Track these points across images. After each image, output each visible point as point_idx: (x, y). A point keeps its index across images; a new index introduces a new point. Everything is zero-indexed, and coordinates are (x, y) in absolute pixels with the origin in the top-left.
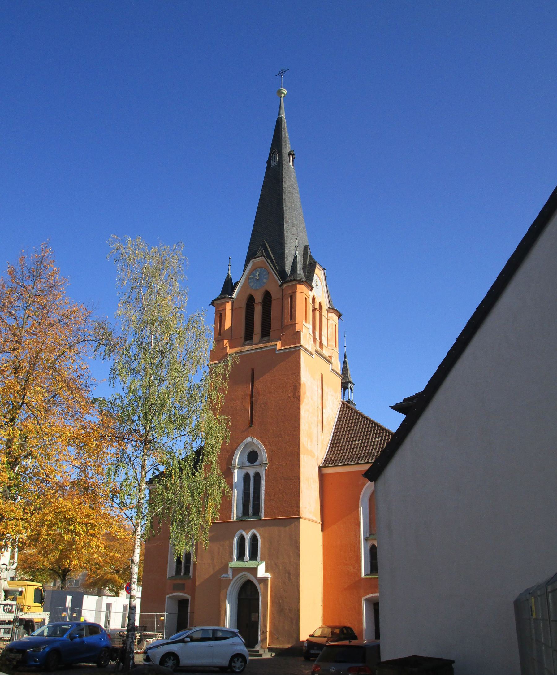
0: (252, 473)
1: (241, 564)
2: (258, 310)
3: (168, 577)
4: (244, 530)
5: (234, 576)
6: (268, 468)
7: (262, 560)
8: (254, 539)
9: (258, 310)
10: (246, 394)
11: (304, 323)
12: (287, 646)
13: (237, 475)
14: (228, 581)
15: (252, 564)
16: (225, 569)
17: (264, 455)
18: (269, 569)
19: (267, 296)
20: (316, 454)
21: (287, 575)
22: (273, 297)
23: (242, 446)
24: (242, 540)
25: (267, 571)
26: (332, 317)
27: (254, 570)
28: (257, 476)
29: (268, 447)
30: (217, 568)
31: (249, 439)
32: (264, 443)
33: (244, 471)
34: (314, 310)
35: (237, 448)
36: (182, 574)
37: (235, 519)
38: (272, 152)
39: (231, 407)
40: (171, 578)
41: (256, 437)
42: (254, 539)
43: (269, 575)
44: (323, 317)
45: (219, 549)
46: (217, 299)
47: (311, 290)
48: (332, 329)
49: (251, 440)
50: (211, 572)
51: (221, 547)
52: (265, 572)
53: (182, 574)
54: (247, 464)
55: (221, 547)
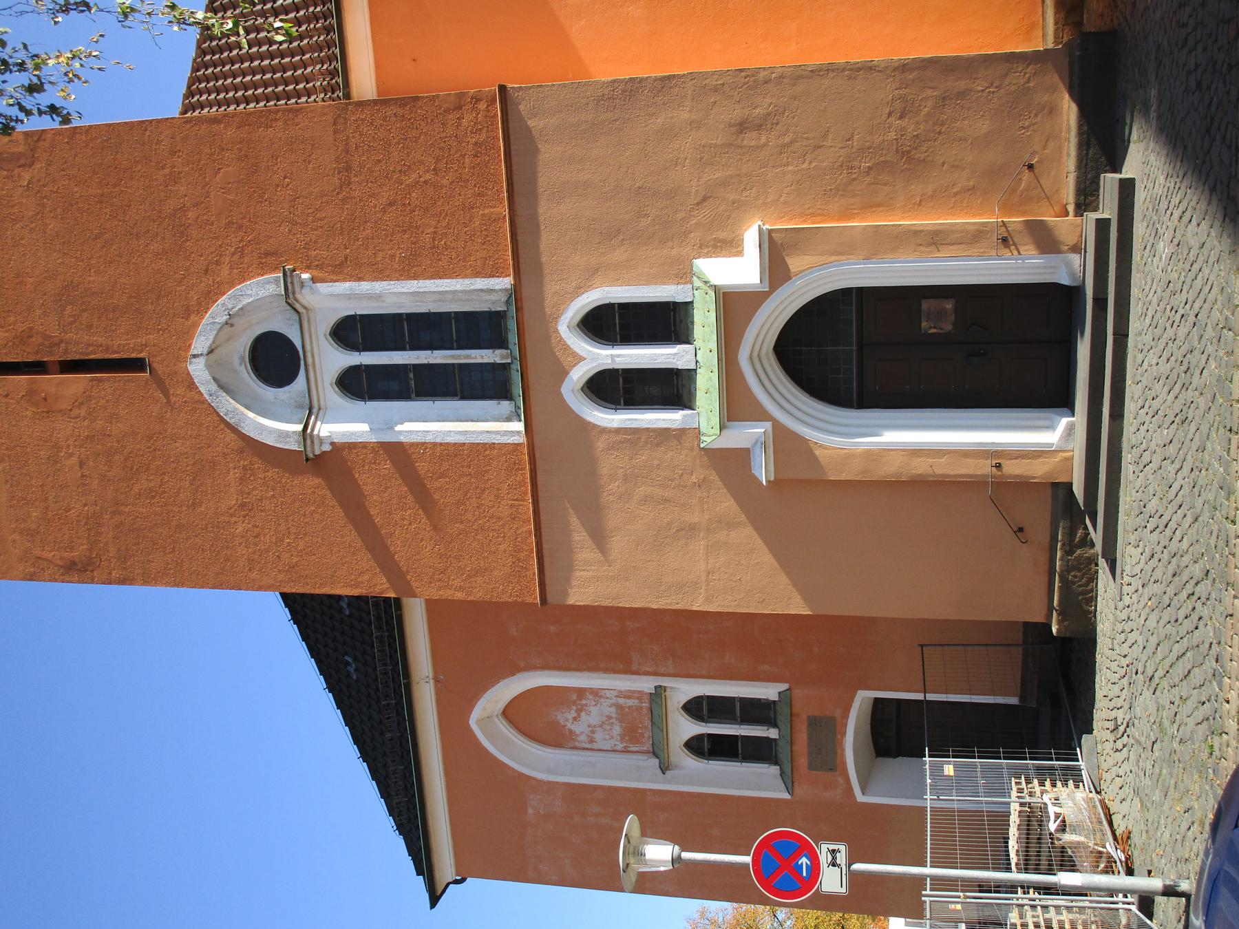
0: (341, 360)
1: (707, 386)
3: (786, 796)
4: (563, 373)
5: (760, 415)
6: (308, 268)
7: (685, 274)
8: (605, 324)
10: (31, 394)
12: (1069, 111)
13: (347, 425)
15: (704, 323)
16: (731, 464)
17: (254, 299)
18: (722, 235)
21: (750, 139)
23: (227, 405)
24: (611, 388)
25: (730, 246)
27: (734, 307)
28: (350, 332)
29: (225, 272)
30: (726, 504)
31: (198, 370)
32: (210, 296)
33: (331, 396)
35: (234, 430)
36: (773, 733)
37: (519, 426)
39: (82, 464)
40: (789, 780)
41: (187, 335)
42: (605, 324)
43: (750, 238)
45: (645, 500)
49: (201, 361)
50: (746, 534)
51: (642, 490)
52: (740, 253)
53: (773, 733)
54: (300, 382)
55: (642, 490)
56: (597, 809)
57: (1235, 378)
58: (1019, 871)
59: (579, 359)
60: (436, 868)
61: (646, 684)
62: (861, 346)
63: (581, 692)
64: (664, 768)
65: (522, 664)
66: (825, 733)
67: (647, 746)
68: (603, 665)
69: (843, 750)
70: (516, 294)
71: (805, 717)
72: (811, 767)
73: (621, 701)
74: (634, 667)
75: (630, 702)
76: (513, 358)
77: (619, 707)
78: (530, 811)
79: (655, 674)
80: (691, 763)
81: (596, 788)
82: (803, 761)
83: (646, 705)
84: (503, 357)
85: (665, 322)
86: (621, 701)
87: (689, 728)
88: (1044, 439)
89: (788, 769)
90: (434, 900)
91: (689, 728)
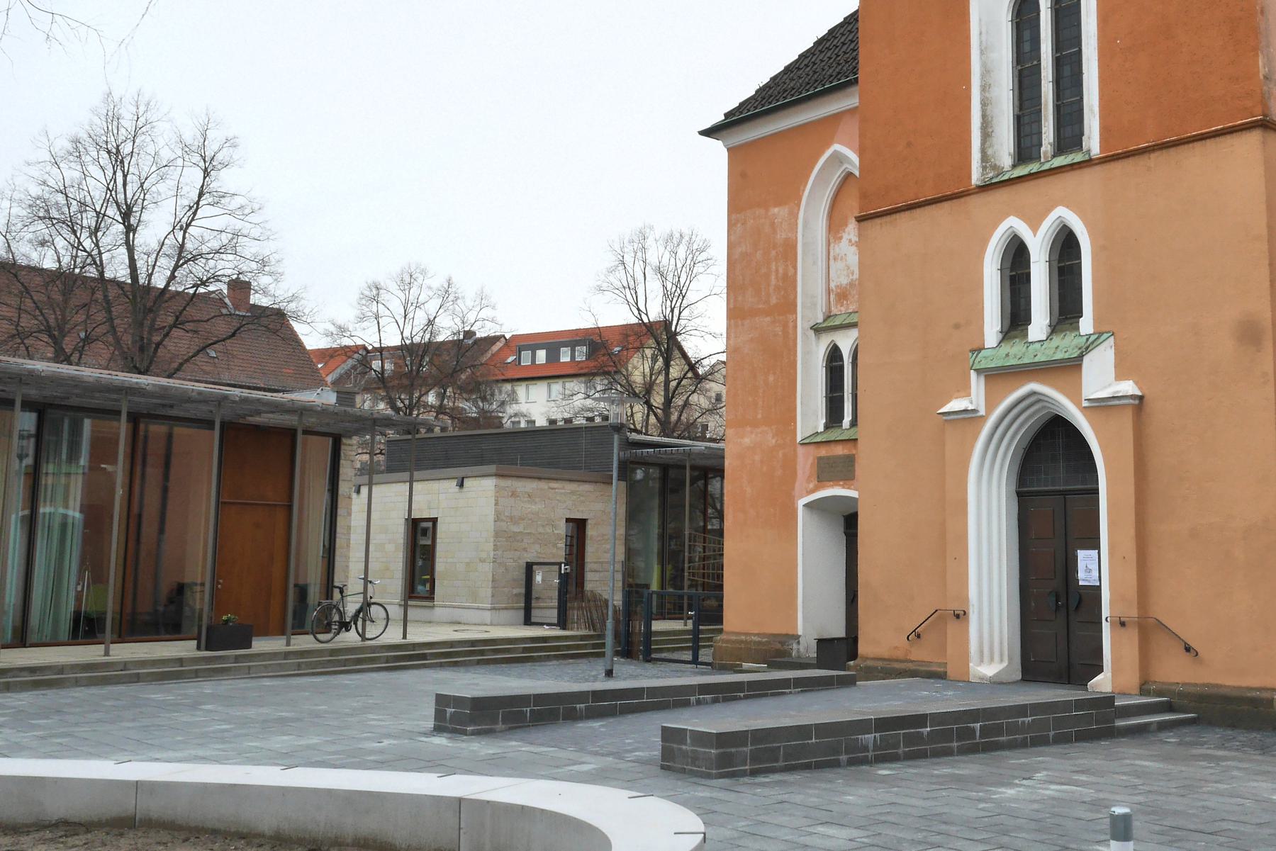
1: (1016, 353)
3: (799, 439)
8: (1066, 245)
14: (969, 418)
15: (1065, 346)
24: (1017, 255)
42: (1066, 245)
56: (781, 271)
57: (261, 850)
59: (1035, 229)
62: (1064, 493)
64: (818, 330)
69: (832, 486)
70: (28, 405)
72: (820, 459)
78: (776, 210)
80: (820, 350)
81: (795, 268)
82: (823, 452)
84: (1045, 153)
85: (1067, 309)
87: (846, 342)
88: (989, 643)
89: (818, 439)
90: (708, 133)
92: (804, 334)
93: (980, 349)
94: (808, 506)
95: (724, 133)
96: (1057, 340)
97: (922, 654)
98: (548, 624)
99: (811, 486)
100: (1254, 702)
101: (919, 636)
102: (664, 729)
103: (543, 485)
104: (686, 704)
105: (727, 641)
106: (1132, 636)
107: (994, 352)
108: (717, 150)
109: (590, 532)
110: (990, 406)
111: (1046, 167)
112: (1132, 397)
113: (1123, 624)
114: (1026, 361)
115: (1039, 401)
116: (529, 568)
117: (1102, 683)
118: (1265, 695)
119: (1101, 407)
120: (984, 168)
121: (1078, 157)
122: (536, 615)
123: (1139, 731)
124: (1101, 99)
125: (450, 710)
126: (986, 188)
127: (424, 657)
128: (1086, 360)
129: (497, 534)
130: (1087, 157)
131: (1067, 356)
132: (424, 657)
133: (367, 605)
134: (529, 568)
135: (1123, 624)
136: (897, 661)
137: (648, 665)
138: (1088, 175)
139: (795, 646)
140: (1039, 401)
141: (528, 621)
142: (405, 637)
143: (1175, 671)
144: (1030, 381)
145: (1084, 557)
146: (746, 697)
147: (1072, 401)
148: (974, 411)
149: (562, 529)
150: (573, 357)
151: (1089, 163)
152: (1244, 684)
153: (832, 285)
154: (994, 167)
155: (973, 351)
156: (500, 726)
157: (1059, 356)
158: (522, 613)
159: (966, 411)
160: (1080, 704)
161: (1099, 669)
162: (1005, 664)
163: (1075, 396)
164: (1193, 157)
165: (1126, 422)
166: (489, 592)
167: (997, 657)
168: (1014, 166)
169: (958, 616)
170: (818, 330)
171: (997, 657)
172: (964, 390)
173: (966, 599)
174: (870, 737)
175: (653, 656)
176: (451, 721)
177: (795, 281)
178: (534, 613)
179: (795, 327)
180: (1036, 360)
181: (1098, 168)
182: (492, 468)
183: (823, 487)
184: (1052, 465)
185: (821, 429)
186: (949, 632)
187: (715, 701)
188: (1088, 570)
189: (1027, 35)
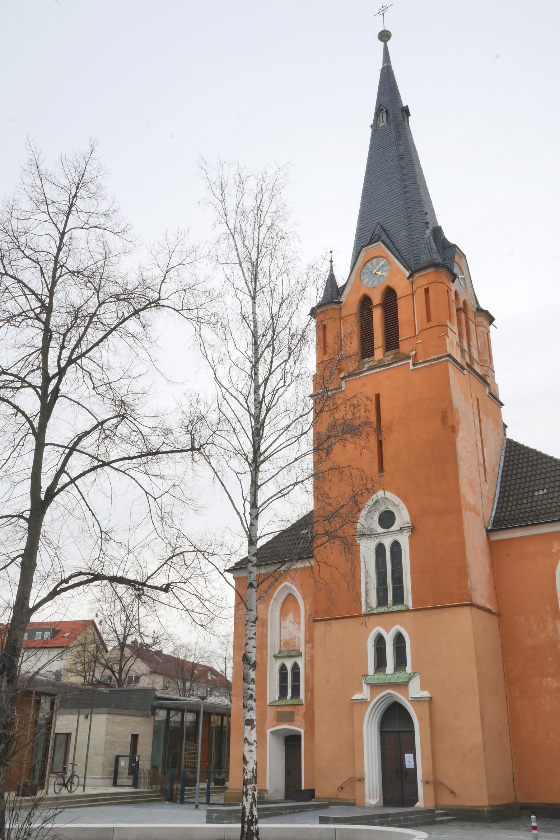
0: (387, 543)
1: (380, 678)
2: (378, 315)
8: (399, 639)
9: (378, 315)
11: (449, 324)
14: (364, 702)
15: (400, 677)
17: (403, 517)
19: (390, 294)
20: (481, 511)
22: (399, 294)
24: (380, 641)
26: (481, 322)
34: (458, 310)
38: (58, 593)
40: (273, 705)
42: (399, 639)
44: (471, 322)
46: (320, 306)
47: (453, 281)
48: (484, 337)
58: (31, 697)
59: (388, 632)
60: (430, 315)
61: (302, 649)
63: (299, 623)
64: (276, 657)
65: (306, 602)
66: (289, 717)
67: (283, 649)
68: (307, 633)
69: (282, 724)
71: (294, 710)
72: (278, 712)
73: (297, 639)
74: (307, 645)
75: (297, 642)
76: (389, 608)
77: (295, 637)
79: (305, 653)
80: (277, 665)
81: (267, 631)
82: (279, 709)
83: (296, 648)
85: (400, 662)
86: (297, 639)
87: (289, 664)
88: (372, 792)
89: (277, 704)
91: (289, 664)
92: (270, 657)
93: (367, 675)
94: (272, 733)
95: (235, 571)
96: (397, 674)
97: (344, 795)
98: (127, 786)
99: (274, 724)
100: (477, 811)
101: (342, 788)
102: (320, 817)
103: (123, 718)
104: (281, 814)
105: (230, 793)
106: (431, 787)
107: (373, 677)
108: (230, 577)
109: (140, 740)
110: (372, 698)
111: (390, 610)
112: (428, 697)
113: (427, 783)
114: (387, 681)
115: (391, 696)
116: (117, 758)
117: (420, 804)
118: (481, 809)
119: (416, 701)
120: (367, 607)
121: (402, 608)
122: (119, 782)
123: (442, 822)
124: (412, 588)
125: (214, 815)
126: (367, 615)
127: (97, 800)
128: (410, 682)
129: (106, 741)
130: (406, 608)
131: (403, 681)
132: (97, 800)
133: (72, 776)
134: (117, 758)
135: (427, 783)
136: (333, 799)
137: (184, 806)
138: (408, 614)
139: (266, 794)
140: (391, 696)
141: (115, 784)
142: (84, 791)
143: (447, 801)
144: (388, 689)
145: (409, 758)
146: (299, 812)
147: (404, 697)
148: (366, 699)
149: (129, 740)
150: (43, 637)
151: (408, 610)
152: (474, 805)
153: (282, 638)
154: (370, 607)
155: (364, 676)
156: (233, 821)
157: (400, 680)
158: (112, 781)
159: (363, 699)
160: (412, 813)
161: (417, 801)
162: (378, 799)
163: (406, 696)
164: (447, 613)
165: (426, 705)
166: (101, 770)
167: (375, 797)
168: (377, 607)
169: (360, 780)
170: (276, 657)
171: (375, 797)
172: (360, 690)
173: (363, 773)
174: (377, 821)
175: (185, 800)
176: (215, 820)
177: (267, 636)
178: (118, 780)
179: (267, 655)
180: (391, 681)
181: (412, 613)
182: (105, 710)
183: (279, 725)
184: (395, 720)
185: (277, 699)
186: (356, 786)
187: (290, 813)
188: (410, 762)
189: (380, 559)
